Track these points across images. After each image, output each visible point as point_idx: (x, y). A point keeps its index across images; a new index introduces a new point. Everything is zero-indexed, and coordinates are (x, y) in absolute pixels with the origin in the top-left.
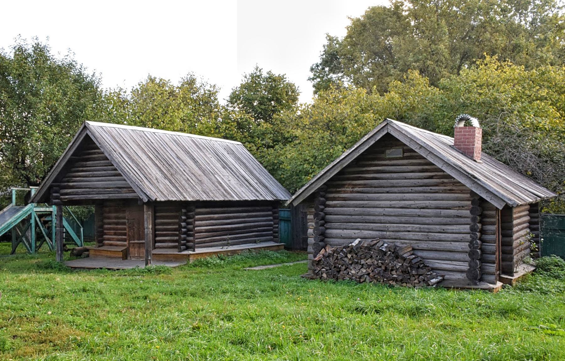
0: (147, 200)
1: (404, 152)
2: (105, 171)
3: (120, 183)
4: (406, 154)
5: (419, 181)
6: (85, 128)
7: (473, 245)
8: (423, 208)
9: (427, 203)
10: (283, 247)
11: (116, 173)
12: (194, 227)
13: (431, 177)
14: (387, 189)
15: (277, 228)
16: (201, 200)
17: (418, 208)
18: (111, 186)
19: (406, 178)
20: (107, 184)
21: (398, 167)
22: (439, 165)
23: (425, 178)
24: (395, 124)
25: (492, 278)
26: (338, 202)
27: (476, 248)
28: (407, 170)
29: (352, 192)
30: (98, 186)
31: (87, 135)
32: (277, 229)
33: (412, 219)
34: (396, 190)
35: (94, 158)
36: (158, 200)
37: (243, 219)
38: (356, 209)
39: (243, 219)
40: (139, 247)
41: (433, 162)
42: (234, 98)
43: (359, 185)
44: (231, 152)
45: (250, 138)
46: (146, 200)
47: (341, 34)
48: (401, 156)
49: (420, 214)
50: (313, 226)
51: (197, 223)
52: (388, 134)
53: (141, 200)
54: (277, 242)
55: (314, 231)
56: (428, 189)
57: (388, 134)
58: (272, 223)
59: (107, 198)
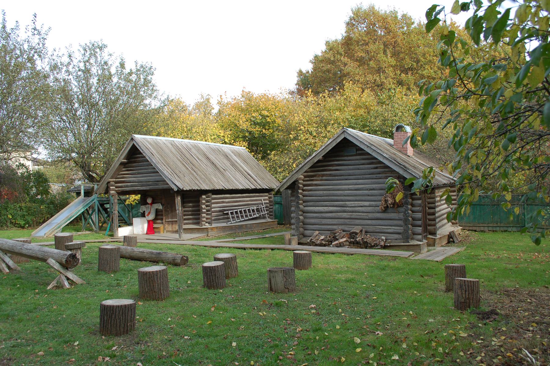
0: (176, 190)
1: (357, 151)
2: (146, 169)
3: (157, 178)
4: (358, 152)
5: (368, 170)
6: (132, 139)
7: (406, 214)
8: (371, 190)
9: (374, 186)
10: (277, 223)
11: (156, 172)
12: (211, 208)
13: (376, 168)
14: (346, 177)
15: (272, 208)
16: (216, 189)
17: (367, 190)
18: (151, 181)
19: (358, 169)
20: (148, 179)
21: (353, 161)
22: (381, 159)
23: (372, 169)
24: (350, 131)
25: (420, 237)
26: (312, 187)
27: (408, 216)
28: (359, 164)
29: (321, 180)
30: (142, 181)
31: (134, 145)
32: (272, 210)
33: (363, 198)
34: (350, 177)
35: (139, 160)
36: (185, 189)
37: (247, 203)
38: (325, 192)
39: (247, 203)
40: (172, 224)
41: (376, 157)
42: (345, 33)
43: (327, 175)
44: (238, 155)
45: (499, 87)
46: (176, 189)
47: (308, 67)
48: (355, 153)
49: (369, 194)
50: (295, 205)
51: (213, 205)
52: (345, 138)
53: (173, 190)
54: (272, 219)
55: (295, 209)
56: (374, 176)
57: (345, 138)
58: (268, 205)
59: (148, 189)
